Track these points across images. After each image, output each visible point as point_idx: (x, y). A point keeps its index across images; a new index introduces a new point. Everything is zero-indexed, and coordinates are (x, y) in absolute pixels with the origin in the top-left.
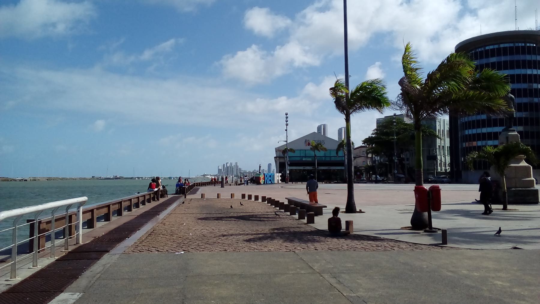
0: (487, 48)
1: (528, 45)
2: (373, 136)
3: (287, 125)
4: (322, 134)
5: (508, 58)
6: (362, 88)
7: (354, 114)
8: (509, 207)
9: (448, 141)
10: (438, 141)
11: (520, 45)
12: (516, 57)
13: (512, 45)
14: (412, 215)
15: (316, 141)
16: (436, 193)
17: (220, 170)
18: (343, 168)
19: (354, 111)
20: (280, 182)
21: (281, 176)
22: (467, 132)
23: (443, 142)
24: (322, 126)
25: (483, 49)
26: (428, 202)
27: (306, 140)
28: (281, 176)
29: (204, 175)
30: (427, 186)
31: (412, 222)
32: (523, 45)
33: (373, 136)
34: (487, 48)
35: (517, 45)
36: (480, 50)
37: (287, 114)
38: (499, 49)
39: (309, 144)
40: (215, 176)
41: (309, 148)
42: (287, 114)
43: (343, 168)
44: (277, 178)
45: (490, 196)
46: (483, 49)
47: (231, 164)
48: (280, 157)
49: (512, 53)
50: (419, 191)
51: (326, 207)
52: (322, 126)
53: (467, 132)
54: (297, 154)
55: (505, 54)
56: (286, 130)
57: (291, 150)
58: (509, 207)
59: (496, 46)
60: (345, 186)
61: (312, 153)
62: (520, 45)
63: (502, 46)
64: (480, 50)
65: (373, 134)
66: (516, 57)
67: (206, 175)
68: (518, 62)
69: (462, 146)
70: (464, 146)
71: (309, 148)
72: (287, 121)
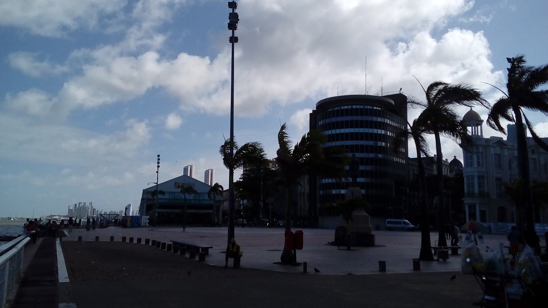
0: (342, 108)
1: (375, 108)
2: (241, 180)
3: (158, 167)
4: (189, 175)
5: (359, 118)
6: (246, 147)
7: (237, 169)
8: (352, 248)
9: (307, 188)
10: (299, 187)
11: (369, 107)
12: (365, 118)
13: (362, 107)
14: (281, 253)
15: (185, 184)
16: (300, 235)
17: (70, 211)
18: (211, 211)
19: (238, 166)
20: (148, 225)
21: (148, 219)
22: (324, 181)
23: (303, 189)
24: (189, 167)
25: (339, 108)
26: (294, 242)
27: (175, 182)
28: (148, 219)
29: (51, 216)
30: (294, 231)
31: (282, 258)
32: (371, 107)
33: (241, 180)
34: (342, 108)
35: (366, 107)
36: (336, 108)
37: (159, 156)
38: (352, 110)
39: (179, 187)
40: (66, 217)
41: (179, 190)
42: (159, 156)
43: (211, 211)
44: (145, 221)
45: (342, 241)
46: (339, 108)
47: (85, 204)
48: (148, 199)
49: (362, 114)
50: (288, 234)
51: (212, 248)
52: (189, 167)
53: (324, 181)
54: (166, 196)
55: (357, 114)
56: (157, 172)
57: (162, 193)
58: (352, 248)
59: (350, 107)
60: (224, 231)
61: (182, 196)
62: (369, 107)
63: (354, 107)
64: (336, 108)
65: (240, 178)
66: (365, 118)
67: (54, 216)
68: (367, 122)
69: (320, 193)
70: (321, 193)
71: (179, 190)
72: (158, 163)
